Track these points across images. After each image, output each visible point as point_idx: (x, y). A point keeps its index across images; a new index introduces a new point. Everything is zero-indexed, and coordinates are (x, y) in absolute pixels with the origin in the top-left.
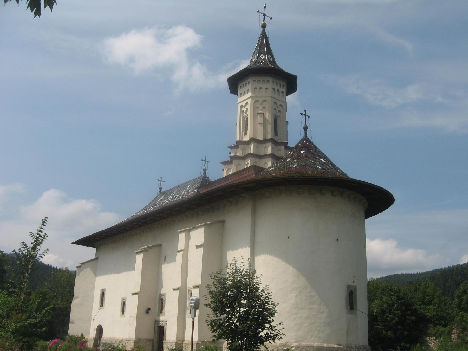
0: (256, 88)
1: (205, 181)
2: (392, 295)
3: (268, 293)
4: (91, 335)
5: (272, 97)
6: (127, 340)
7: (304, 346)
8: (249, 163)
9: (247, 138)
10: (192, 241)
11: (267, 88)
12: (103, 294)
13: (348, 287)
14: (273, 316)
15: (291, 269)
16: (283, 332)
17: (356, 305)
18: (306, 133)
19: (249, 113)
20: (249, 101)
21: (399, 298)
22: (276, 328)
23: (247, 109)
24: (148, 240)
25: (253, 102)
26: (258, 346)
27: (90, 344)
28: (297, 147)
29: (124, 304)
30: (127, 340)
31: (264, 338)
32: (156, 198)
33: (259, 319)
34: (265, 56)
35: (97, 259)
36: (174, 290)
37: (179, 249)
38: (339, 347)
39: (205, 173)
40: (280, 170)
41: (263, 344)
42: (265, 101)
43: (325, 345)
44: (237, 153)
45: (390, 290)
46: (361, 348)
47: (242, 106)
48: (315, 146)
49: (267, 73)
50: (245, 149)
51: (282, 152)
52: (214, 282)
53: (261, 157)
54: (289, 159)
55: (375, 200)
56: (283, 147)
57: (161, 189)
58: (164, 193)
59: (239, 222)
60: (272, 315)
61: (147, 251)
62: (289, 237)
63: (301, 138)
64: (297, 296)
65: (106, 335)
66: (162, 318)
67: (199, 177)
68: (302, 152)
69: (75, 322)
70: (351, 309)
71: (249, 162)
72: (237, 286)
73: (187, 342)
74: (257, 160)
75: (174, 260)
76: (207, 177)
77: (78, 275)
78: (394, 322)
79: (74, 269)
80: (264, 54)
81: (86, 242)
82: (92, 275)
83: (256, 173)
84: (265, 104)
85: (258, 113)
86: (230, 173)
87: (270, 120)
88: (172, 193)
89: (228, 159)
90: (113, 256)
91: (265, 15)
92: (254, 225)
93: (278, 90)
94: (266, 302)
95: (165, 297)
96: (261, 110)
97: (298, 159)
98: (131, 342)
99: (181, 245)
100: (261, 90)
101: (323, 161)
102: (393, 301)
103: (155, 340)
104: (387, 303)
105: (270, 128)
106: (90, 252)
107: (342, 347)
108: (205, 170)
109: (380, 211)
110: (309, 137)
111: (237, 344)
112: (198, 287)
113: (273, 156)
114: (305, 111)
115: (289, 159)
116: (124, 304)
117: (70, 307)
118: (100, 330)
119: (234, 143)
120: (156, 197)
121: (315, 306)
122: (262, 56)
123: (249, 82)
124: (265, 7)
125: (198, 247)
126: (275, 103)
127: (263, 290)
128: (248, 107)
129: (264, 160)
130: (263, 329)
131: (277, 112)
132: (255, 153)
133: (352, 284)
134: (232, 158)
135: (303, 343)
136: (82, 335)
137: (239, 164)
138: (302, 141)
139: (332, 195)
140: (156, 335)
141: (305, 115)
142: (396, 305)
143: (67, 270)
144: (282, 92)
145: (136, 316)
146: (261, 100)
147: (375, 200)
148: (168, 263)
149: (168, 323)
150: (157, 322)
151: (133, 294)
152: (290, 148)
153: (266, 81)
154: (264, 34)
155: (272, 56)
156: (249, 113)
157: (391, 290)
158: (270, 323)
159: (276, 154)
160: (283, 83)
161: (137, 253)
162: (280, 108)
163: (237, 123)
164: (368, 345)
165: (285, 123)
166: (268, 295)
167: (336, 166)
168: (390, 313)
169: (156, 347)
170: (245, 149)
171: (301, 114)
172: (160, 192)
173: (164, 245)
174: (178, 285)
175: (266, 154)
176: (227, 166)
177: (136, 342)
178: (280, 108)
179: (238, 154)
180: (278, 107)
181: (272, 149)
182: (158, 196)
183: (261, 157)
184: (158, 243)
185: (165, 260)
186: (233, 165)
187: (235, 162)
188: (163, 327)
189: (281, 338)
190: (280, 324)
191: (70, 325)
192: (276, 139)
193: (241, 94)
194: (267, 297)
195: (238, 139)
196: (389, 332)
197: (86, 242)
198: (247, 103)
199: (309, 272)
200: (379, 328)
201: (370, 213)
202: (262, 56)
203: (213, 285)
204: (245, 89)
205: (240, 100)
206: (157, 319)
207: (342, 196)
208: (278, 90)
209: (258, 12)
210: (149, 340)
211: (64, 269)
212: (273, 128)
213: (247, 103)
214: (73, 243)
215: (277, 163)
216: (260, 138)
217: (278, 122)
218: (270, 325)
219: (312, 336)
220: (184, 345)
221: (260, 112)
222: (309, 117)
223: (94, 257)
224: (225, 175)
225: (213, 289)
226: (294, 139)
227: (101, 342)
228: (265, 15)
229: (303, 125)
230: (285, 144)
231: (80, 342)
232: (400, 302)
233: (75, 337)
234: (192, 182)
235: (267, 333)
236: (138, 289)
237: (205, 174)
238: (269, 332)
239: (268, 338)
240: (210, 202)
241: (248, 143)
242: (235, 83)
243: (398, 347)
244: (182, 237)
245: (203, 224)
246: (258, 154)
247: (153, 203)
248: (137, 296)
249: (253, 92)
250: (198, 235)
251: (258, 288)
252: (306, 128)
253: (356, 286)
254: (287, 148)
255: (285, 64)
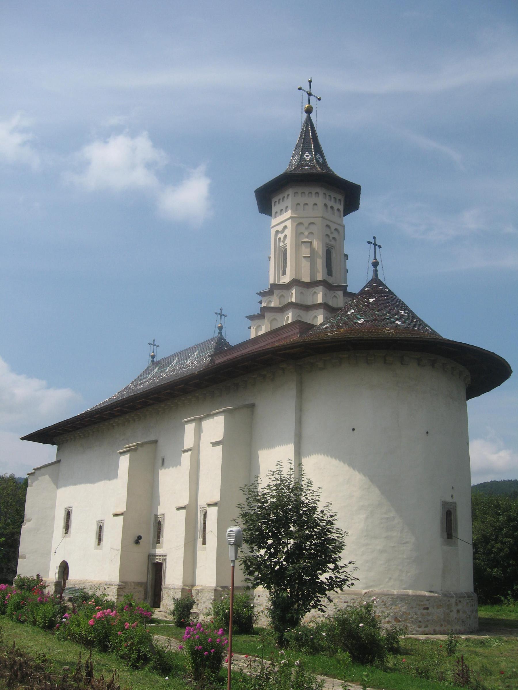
0: (298, 204)
1: (221, 345)
2: (499, 515)
3: (331, 516)
4: (52, 576)
5: (322, 217)
6: (106, 585)
7: (379, 594)
8: (289, 317)
9: (286, 280)
10: (207, 433)
11: (316, 204)
12: (68, 515)
13: (444, 504)
14: (340, 552)
15: (358, 477)
16: (355, 575)
17: (456, 530)
18: (376, 271)
19: (288, 241)
20: (288, 223)
21: (510, 519)
22: (344, 569)
23: (286, 236)
24: (137, 434)
25: (296, 224)
26: (317, 597)
27: (50, 590)
28: (363, 292)
29: (100, 530)
30: (106, 585)
31: (326, 585)
32: (147, 371)
33: (317, 556)
34: (312, 156)
35: (58, 462)
36: (178, 509)
37: (186, 447)
38: (432, 594)
39: (220, 333)
40: (338, 327)
41: (326, 595)
42: (313, 223)
43: (410, 592)
44: (270, 301)
45: (496, 507)
46: (465, 597)
47: (277, 232)
48: (389, 290)
49: (315, 181)
50: (282, 296)
51: (339, 301)
52: (247, 499)
53: (308, 308)
54: (353, 311)
55: (481, 371)
56: (340, 293)
57: (153, 357)
58: (158, 363)
59: (277, 406)
60: (339, 548)
61: (135, 450)
62: (353, 430)
63: (369, 279)
64: (367, 518)
65: (75, 576)
66: (158, 551)
67: (213, 339)
68: (371, 300)
69: (27, 556)
70: (448, 538)
71: (290, 315)
72: (281, 504)
73: (198, 588)
74: (302, 313)
75: (177, 463)
76: (223, 339)
77: (31, 486)
78: (502, 554)
79: (26, 476)
80: (310, 153)
81: (42, 436)
82: (53, 486)
83: (301, 333)
84: (313, 228)
85: (303, 242)
86: (260, 333)
87: (320, 253)
88: (170, 363)
89: (258, 312)
90: (81, 458)
91: (310, 94)
92: (300, 411)
93: (332, 207)
94: (328, 529)
95: (163, 520)
96: (307, 237)
97: (365, 310)
98: (113, 587)
99: (189, 441)
100: (306, 206)
101: (403, 313)
102: (500, 522)
103: (149, 584)
104: (492, 526)
105: (320, 263)
106: (48, 452)
107: (436, 595)
108: (220, 328)
109: (488, 388)
110: (381, 277)
111: (285, 595)
112: (215, 504)
113: (325, 306)
114: (374, 238)
115: (353, 311)
116: (100, 530)
117: (20, 533)
118: (64, 568)
119: (267, 288)
120: (147, 370)
121: (395, 534)
122: (307, 156)
123: (288, 195)
124: (310, 82)
125: (215, 444)
126: (328, 226)
127: (322, 512)
128: (288, 232)
129: (313, 313)
130: (324, 571)
131: (330, 241)
132: (299, 302)
133: (449, 499)
134: (263, 309)
135: (377, 590)
136: (38, 576)
137: (275, 319)
138: (370, 284)
139: (419, 365)
140: (150, 577)
141: (375, 244)
142: (505, 530)
143: (12, 479)
144: (338, 210)
145: (120, 548)
146: (306, 222)
147: (481, 371)
148: (167, 468)
149: (168, 558)
150: (151, 556)
151: (115, 515)
152: (352, 295)
153: (313, 194)
154: (309, 122)
155: (322, 156)
156: (288, 241)
157: (498, 506)
158: (334, 561)
159: (330, 304)
160: (339, 197)
161: (121, 453)
162: (336, 235)
163: (270, 258)
164: (473, 591)
165: (343, 256)
166: (331, 519)
167: (422, 321)
168: (496, 540)
169: (150, 594)
170: (282, 296)
171: (369, 243)
172: (153, 361)
173: (161, 442)
174: (185, 502)
175: (315, 303)
176: (256, 321)
177: (121, 588)
178: (336, 235)
179: (272, 304)
180: (332, 233)
181: (325, 295)
182: (149, 367)
183: (308, 308)
184: (152, 438)
185: (163, 464)
186: (266, 320)
187: (267, 315)
188: (162, 564)
189: (352, 584)
190: (350, 563)
191: (20, 561)
192: (331, 280)
193: (276, 212)
194: (329, 521)
195: (272, 282)
196: (496, 570)
197: (42, 436)
198: (285, 227)
199: (386, 483)
200: (481, 564)
201: (475, 390)
202: (307, 156)
203: (246, 503)
204: (282, 205)
205: (274, 221)
206: (152, 552)
207: (433, 366)
208: (332, 207)
209: (300, 89)
210: (139, 584)
211: (8, 476)
212: (325, 264)
213: (285, 227)
214: (23, 439)
215: (334, 318)
216: (306, 279)
217: (332, 256)
218: (336, 565)
219: (390, 579)
220: (194, 592)
221: (306, 240)
222: (380, 247)
223: (54, 460)
224: (253, 336)
225: (247, 509)
226: (357, 280)
227: (67, 586)
228: (310, 94)
229: (372, 260)
230: (344, 288)
231: (35, 585)
232: (511, 524)
233: (28, 579)
234: (201, 346)
235: (331, 577)
236: (123, 508)
237: (221, 335)
238: (333, 576)
239: (333, 584)
240: (231, 377)
241: (287, 287)
242: (267, 197)
243: (509, 592)
244: (190, 429)
245: (222, 409)
246: (302, 303)
247: (141, 378)
248: (121, 518)
249: (295, 210)
250: (215, 427)
251: (315, 508)
252: (375, 264)
253: (455, 503)
254: (347, 294)
255: (341, 168)
